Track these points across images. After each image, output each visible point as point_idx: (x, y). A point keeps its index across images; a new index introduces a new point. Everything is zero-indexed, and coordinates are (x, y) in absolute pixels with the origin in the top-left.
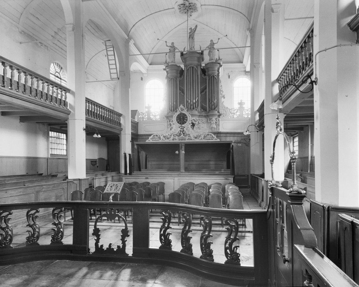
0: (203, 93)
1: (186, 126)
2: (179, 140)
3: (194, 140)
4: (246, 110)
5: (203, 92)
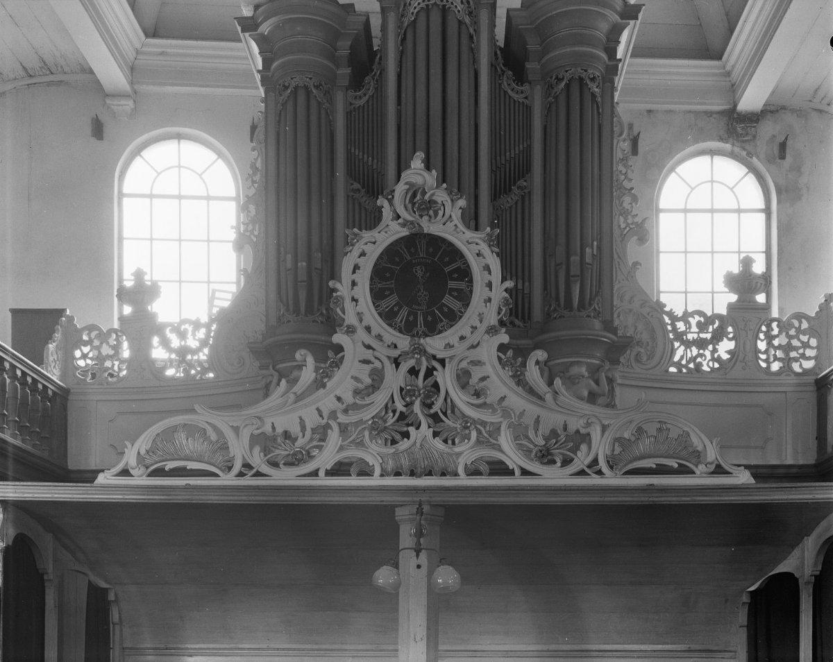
0: (507, 201)
1: (460, 348)
2: (398, 474)
3: (525, 472)
4: (774, 325)
5: (508, 191)
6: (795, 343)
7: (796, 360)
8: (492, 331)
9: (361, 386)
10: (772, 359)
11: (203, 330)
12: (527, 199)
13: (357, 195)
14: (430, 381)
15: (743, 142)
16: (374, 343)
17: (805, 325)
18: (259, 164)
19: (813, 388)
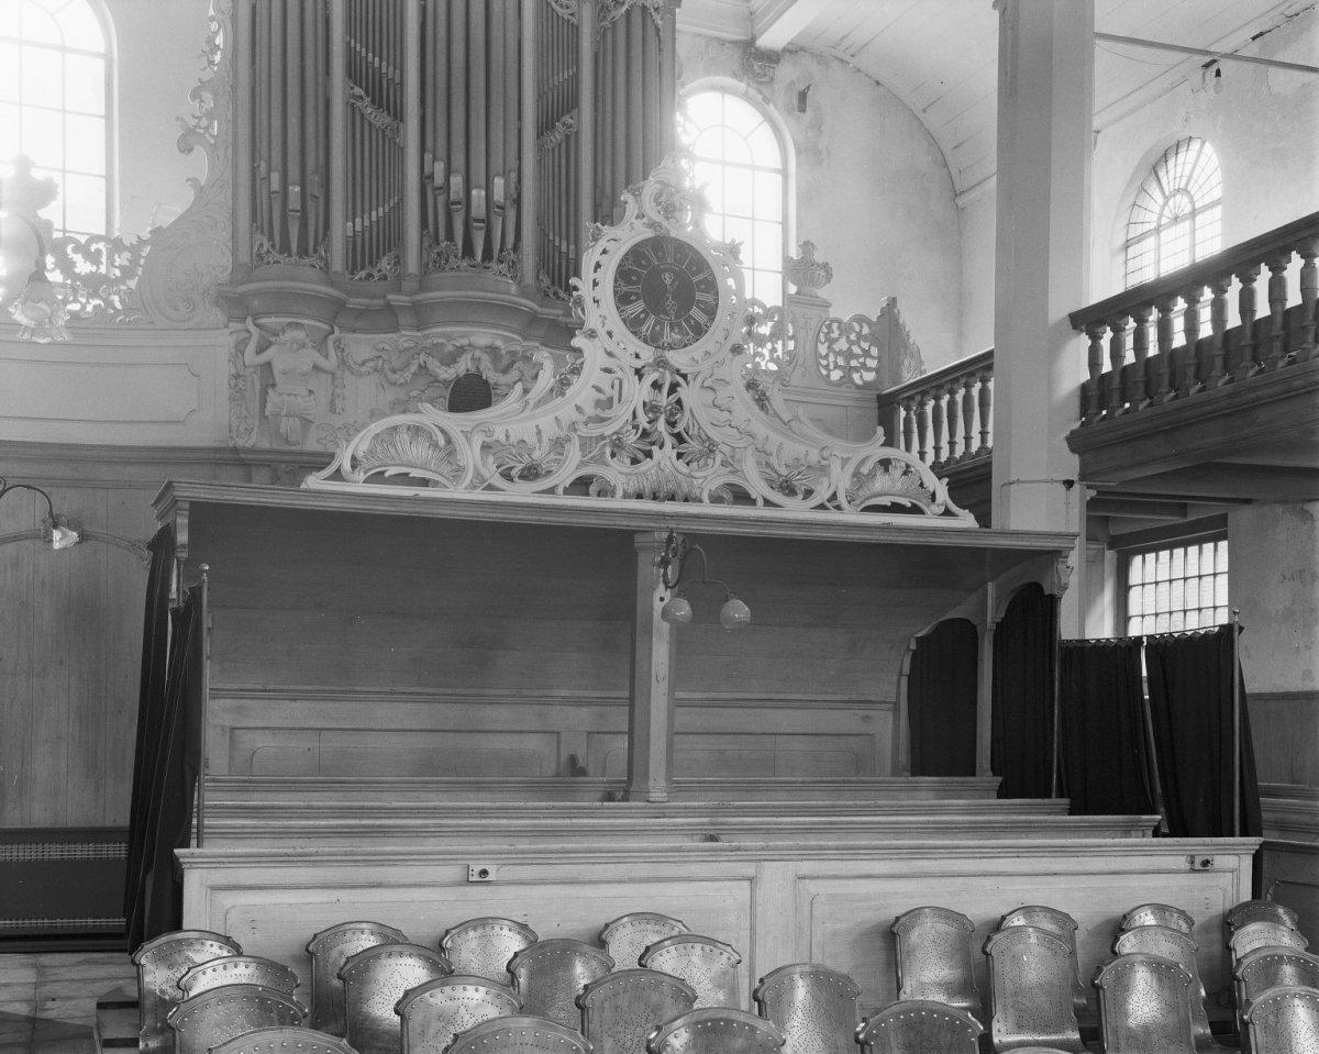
2: (639, 496)
3: (767, 503)
4: (835, 326)
6: (856, 350)
7: (856, 369)
9: (601, 396)
10: (831, 367)
11: (127, 255)
12: (572, 140)
13: (359, 104)
14: (673, 398)
15: (761, 83)
16: (616, 351)
17: (866, 330)
18: (219, 40)
19: (876, 405)
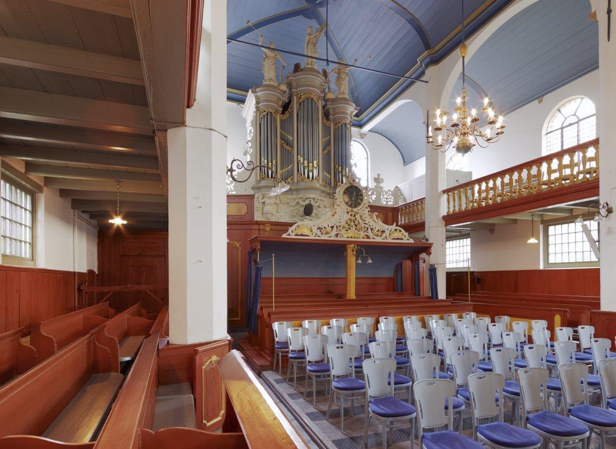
3: (373, 238)
6: (388, 197)
8: (366, 208)
18: (252, 131)
